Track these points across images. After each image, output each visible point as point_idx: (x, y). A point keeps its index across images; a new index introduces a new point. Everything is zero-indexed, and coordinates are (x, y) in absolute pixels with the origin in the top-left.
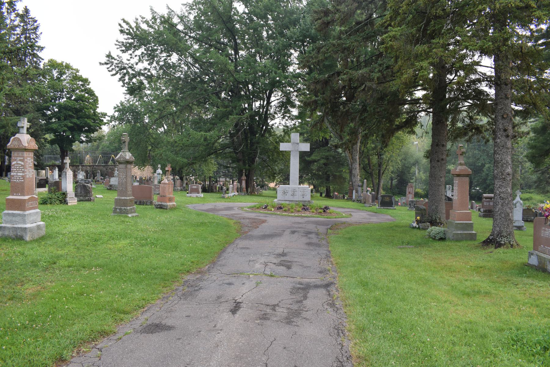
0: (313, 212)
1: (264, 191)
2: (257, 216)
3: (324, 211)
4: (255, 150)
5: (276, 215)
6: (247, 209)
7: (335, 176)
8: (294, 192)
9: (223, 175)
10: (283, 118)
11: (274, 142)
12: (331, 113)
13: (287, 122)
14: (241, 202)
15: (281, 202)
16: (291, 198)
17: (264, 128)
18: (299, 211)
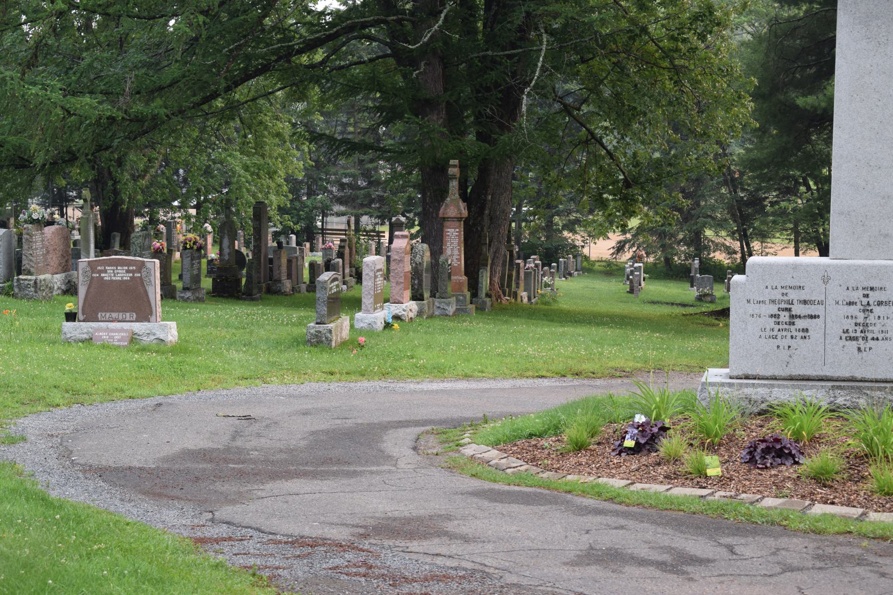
1: (560, 283)
4: (513, 46)
6: (493, 454)
8: (867, 310)
9: (340, 201)
14: (439, 372)
15: (758, 391)
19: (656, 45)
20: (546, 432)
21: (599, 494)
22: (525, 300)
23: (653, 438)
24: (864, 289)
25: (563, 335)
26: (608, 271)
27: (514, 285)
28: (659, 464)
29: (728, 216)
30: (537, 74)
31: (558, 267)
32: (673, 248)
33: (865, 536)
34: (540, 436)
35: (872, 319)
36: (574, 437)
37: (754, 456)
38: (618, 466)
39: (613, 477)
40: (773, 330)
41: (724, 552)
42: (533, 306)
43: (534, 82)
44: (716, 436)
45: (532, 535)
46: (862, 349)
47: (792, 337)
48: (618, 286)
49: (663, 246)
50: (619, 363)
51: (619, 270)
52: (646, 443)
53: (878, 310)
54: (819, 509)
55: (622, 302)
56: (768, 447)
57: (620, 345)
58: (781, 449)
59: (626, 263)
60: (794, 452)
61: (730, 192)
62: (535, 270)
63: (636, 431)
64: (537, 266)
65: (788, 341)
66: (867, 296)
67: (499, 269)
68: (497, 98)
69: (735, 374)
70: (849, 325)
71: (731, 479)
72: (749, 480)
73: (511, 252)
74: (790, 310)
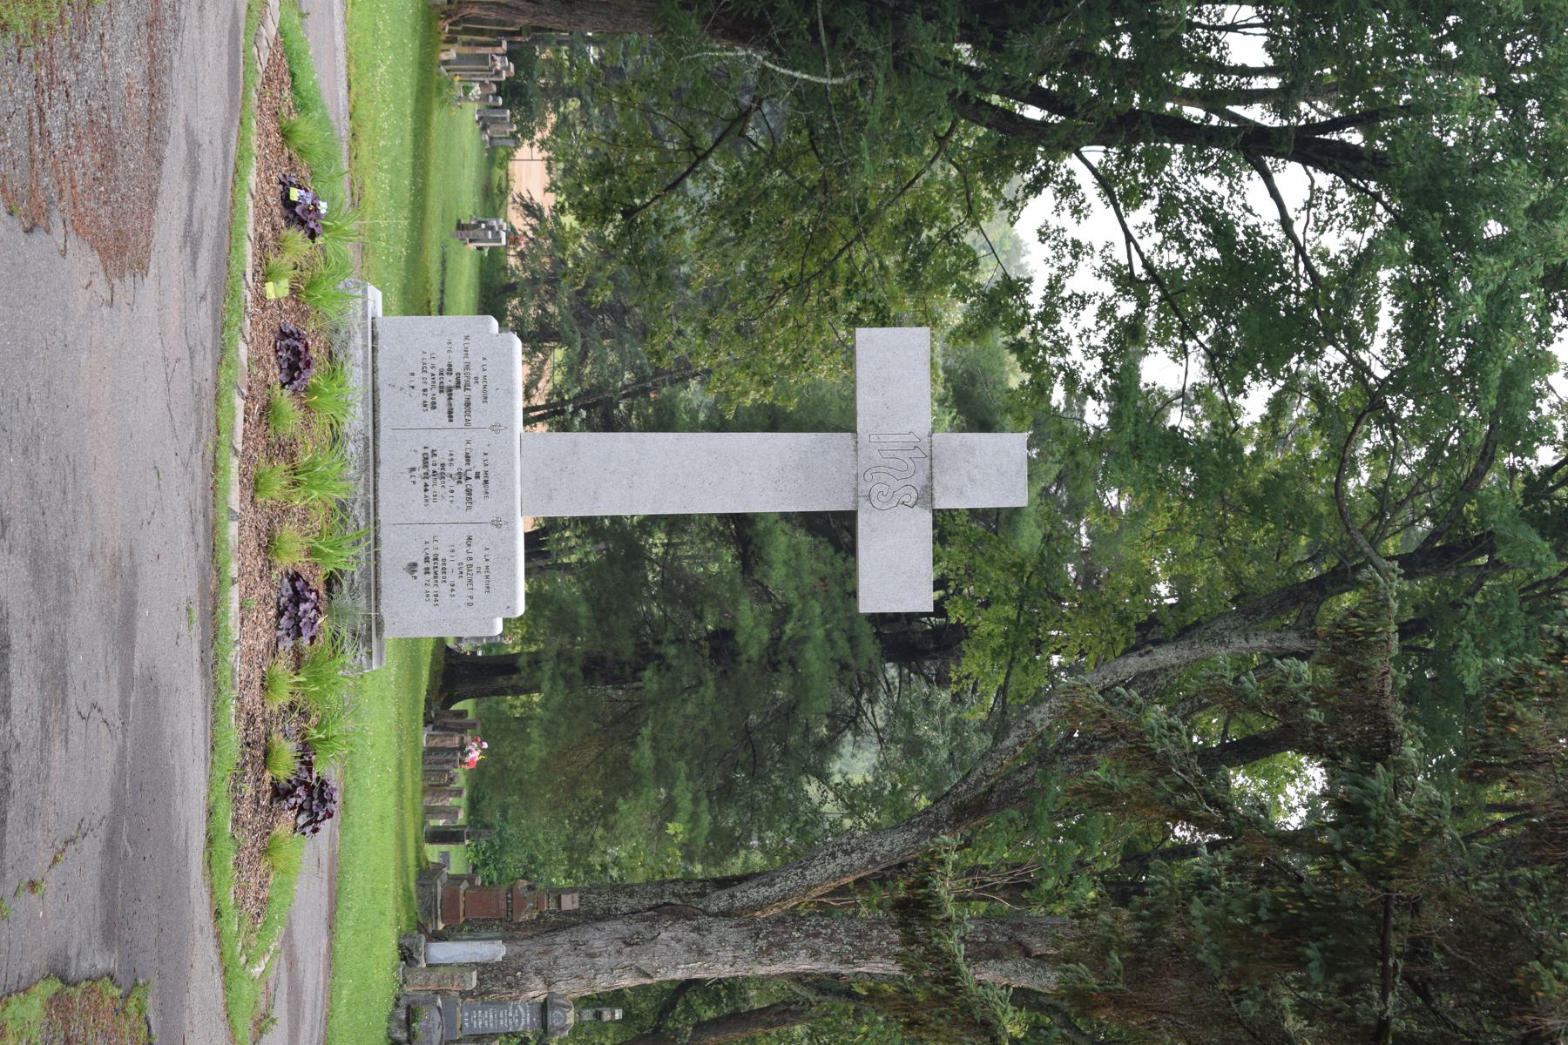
0: (266, 685)
1: (470, 113)
2: (194, 145)
3: (280, 793)
4: (833, 33)
5: (221, 327)
6: (271, 30)
7: (624, 723)
8: (461, 477)
10: (1125, 281)
11: (907, 203)
12: (1276, 909)
13: (1089, 315)
15: (358, 349)
16: (397, 453)
17: (1034, 113)
18: (269, 546)
19: (841, 251)
20: (298, 94)
21: (241, 157)
22: (444, 57)
23: (303, 223)
24: (486, 472)
25: (403, 114)
26: (492, 190)
27: (465, 38)
28: (273, 229)
29: (586, 386)
30: (782, 71)
31: (496, 107)
32: (532, 298)
33: (216, 449)
34: (293, 88)
35: (449, 483)
36: (298, 128)
37: (288, 337)
38: (269, 181)
39: (258, 175)
40: (433, 367)
41: (201, 290)
42: (435, 70)
43: (771, 66)
44: (309, 296)
45: (207, 80)
46: (414, 473)
47: (425, 390)
48: (468, 206)
49: (534, 281)
50: (370, 192)
51: (494, 208)
52: (295, 214)
53: (460, 490)
54: (239, 403)
55: (444, 210)
56: (299, 353)
57: (392, 197)
58: (298, 368)
59: (505, 220)
60: (295, 383)
61: (625, 387)
62: (490, 70)
63: (309, 202)
64: (498, 73)
65: (420, 386)
66: (477, 476)
67: (493, 15)
68: (752, 10)
69: (378, 325)
70: (442, 457)
71: (263, 309)
72: (264, 330)
73: (519, 33)
74: (458, 387)
